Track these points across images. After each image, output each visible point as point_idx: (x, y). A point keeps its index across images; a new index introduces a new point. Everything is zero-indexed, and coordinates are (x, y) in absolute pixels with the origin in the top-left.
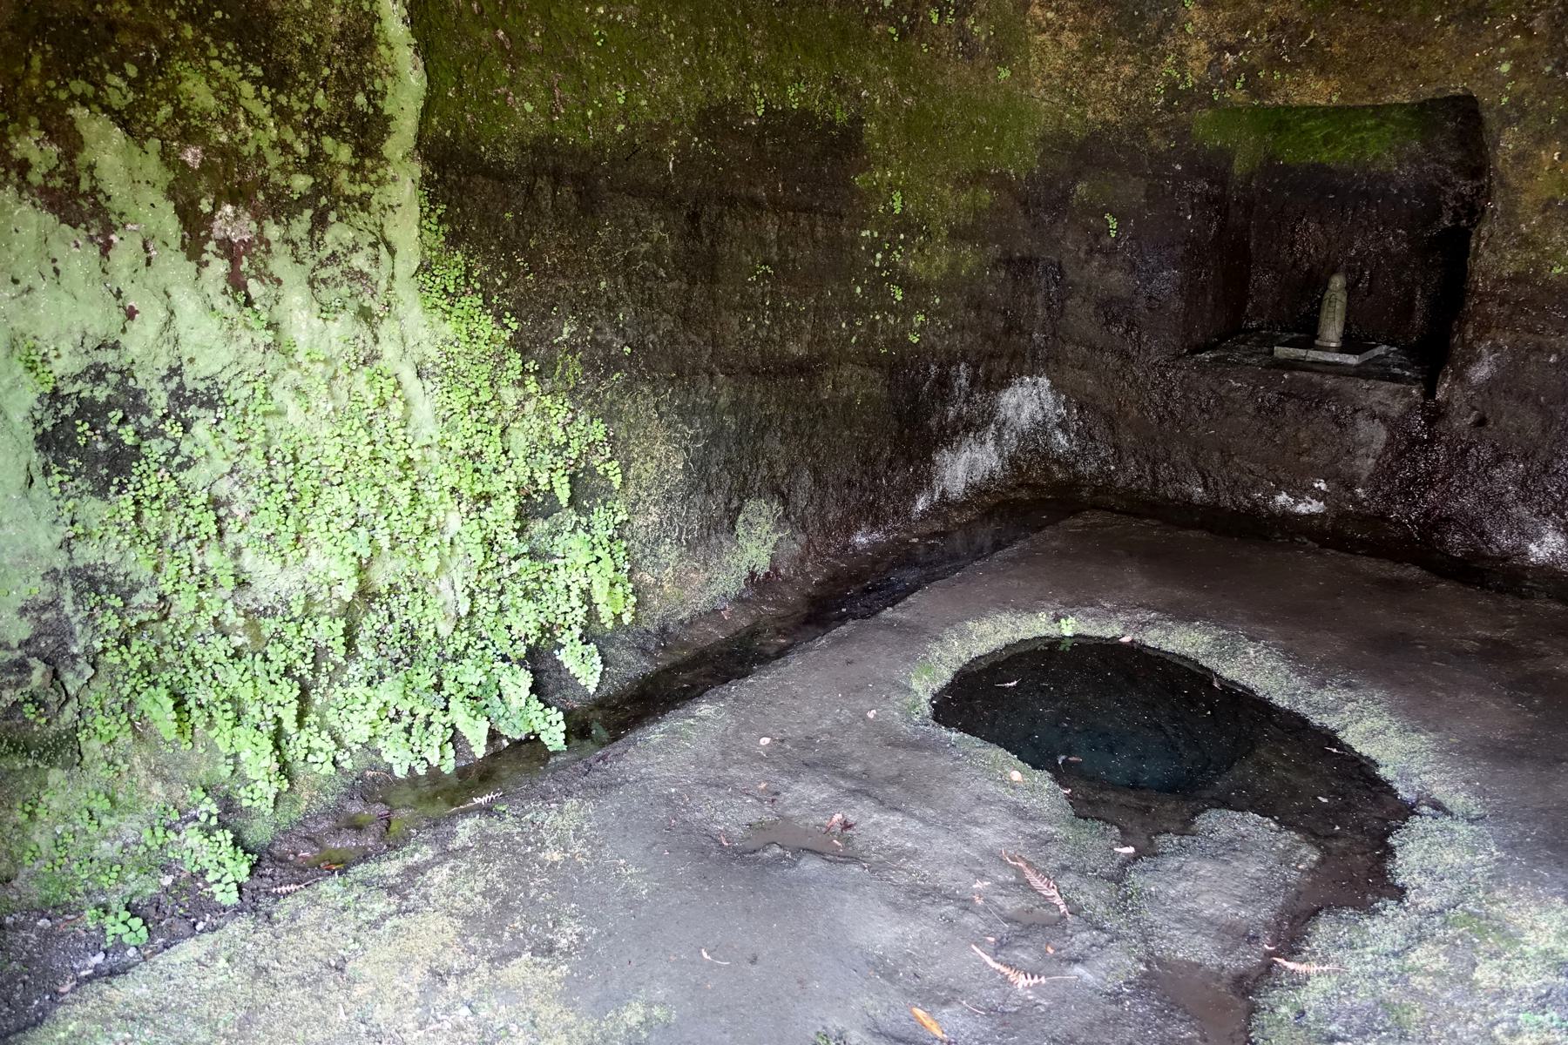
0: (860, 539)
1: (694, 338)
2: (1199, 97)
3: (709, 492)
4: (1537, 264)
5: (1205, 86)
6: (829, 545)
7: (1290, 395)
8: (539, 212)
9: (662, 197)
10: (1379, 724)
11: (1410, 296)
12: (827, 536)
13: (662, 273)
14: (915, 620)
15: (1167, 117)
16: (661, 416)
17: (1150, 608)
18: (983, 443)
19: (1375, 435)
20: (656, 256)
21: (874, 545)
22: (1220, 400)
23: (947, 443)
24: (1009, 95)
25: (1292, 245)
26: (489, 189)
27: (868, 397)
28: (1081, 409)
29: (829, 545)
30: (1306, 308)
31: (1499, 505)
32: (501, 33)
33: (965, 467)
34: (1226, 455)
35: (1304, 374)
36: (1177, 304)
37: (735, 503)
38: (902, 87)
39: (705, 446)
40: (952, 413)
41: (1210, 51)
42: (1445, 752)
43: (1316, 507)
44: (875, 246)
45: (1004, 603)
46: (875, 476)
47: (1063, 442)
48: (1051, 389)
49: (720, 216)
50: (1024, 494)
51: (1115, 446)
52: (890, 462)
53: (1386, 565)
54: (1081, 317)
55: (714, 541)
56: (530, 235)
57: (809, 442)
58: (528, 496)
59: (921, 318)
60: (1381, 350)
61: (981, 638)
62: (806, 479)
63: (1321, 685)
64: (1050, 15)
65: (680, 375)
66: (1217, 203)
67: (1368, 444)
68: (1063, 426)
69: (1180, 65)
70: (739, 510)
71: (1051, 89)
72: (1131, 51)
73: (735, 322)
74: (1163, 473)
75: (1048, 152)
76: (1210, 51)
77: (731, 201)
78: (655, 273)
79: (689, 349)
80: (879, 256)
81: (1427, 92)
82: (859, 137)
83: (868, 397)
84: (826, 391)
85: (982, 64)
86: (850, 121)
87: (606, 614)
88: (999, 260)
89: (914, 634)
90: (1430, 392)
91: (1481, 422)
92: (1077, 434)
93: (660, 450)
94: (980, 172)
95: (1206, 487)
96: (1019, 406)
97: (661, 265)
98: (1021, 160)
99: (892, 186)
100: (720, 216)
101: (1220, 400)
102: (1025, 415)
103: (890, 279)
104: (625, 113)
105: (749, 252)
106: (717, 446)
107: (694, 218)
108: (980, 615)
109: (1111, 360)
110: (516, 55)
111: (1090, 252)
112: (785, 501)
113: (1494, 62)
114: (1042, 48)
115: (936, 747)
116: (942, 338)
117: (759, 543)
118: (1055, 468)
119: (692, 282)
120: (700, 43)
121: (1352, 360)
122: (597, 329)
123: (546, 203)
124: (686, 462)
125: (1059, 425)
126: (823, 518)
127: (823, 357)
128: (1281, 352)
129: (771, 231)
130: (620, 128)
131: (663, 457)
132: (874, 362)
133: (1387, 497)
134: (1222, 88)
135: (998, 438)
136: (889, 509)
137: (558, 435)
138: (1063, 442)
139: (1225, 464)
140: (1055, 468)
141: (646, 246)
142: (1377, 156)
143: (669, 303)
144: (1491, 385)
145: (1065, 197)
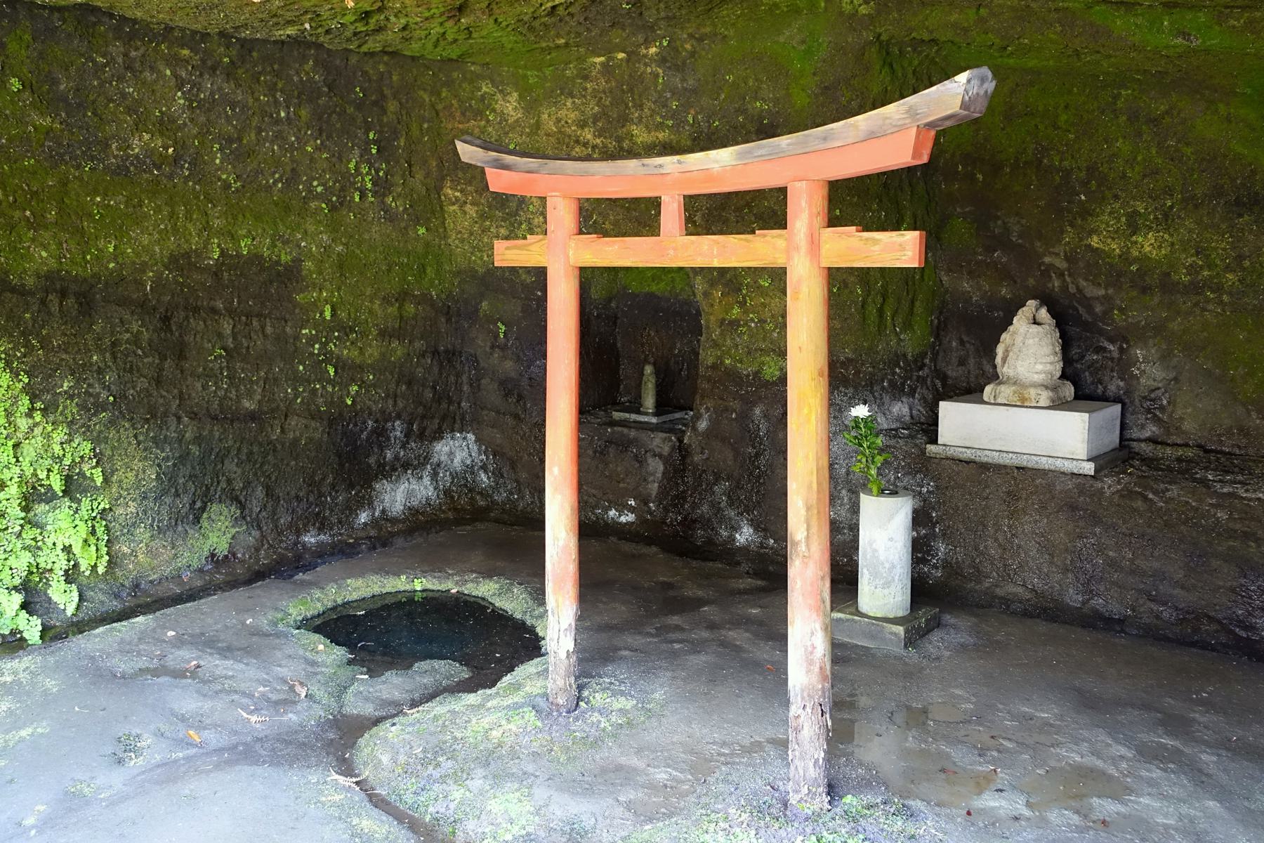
1: (165, 394)
3: (177, 495)
6: (281, 541)
7: (611, 442)
8: (49, 313)
9: (142, 307)
13: (140, 352)
16: (139, 443)
17: (472, 571)
18: (421, 478)
19: (656, 467)
20: (136, 340)
23: (387, 476)
26: (14, 300)
27: (311, 439)
28: (494, 456)
32: (28, 213)
33: (400, 495)
35: (620, 429)
37: (199, 504)
39: (174, 465)
40: (389, 455)
43: (627, 518)
44: (311, 341)
46: (321, 495)
49: (187, 318)
51: (517, 481)
52: (333, 486)
55: (180, 528)
56: (43, 327)
57: (261, 467)
58: (34, 488)
62: (260, 492)
64: (458, 194)
65: (154, 416)
68: (484, 467)
70: (203, 509)
72: (504, 220)
73: (199, 386)
77: (196, 310)
78: (134, 352)
79: (161, 401)
80: (317, 346)
82: (299, 271)
83: (311, 439)
85: (403, 225)
86: (293, 261)
87: (84, 566)
88: (426, 351)
93: (138, 465)
97: (138, 347)
100: (187, 318)
102: (457, 460)
104: (115, 257)
105: (210, 341)
106: (184, 465)
107: (166, 319)
109: (509, 420)
110: (37, 224)
111: (492, 347)
112: (242, 507)
117: (220, 533)
119: (163, 358)
120: (172, 215)
122: (89, 385)
123: (55, 308)
124: (158, 475)
125: (482, 467)
128: (617, 415)
129: (227, 327)
130: (112, 265)
131: (138, 471)
135: (434, 476)
136: (334, 520)
137: (57, 449)
141: (128, 335)
142: (682, 289)
143: (145, 371)
144: (708, 434)
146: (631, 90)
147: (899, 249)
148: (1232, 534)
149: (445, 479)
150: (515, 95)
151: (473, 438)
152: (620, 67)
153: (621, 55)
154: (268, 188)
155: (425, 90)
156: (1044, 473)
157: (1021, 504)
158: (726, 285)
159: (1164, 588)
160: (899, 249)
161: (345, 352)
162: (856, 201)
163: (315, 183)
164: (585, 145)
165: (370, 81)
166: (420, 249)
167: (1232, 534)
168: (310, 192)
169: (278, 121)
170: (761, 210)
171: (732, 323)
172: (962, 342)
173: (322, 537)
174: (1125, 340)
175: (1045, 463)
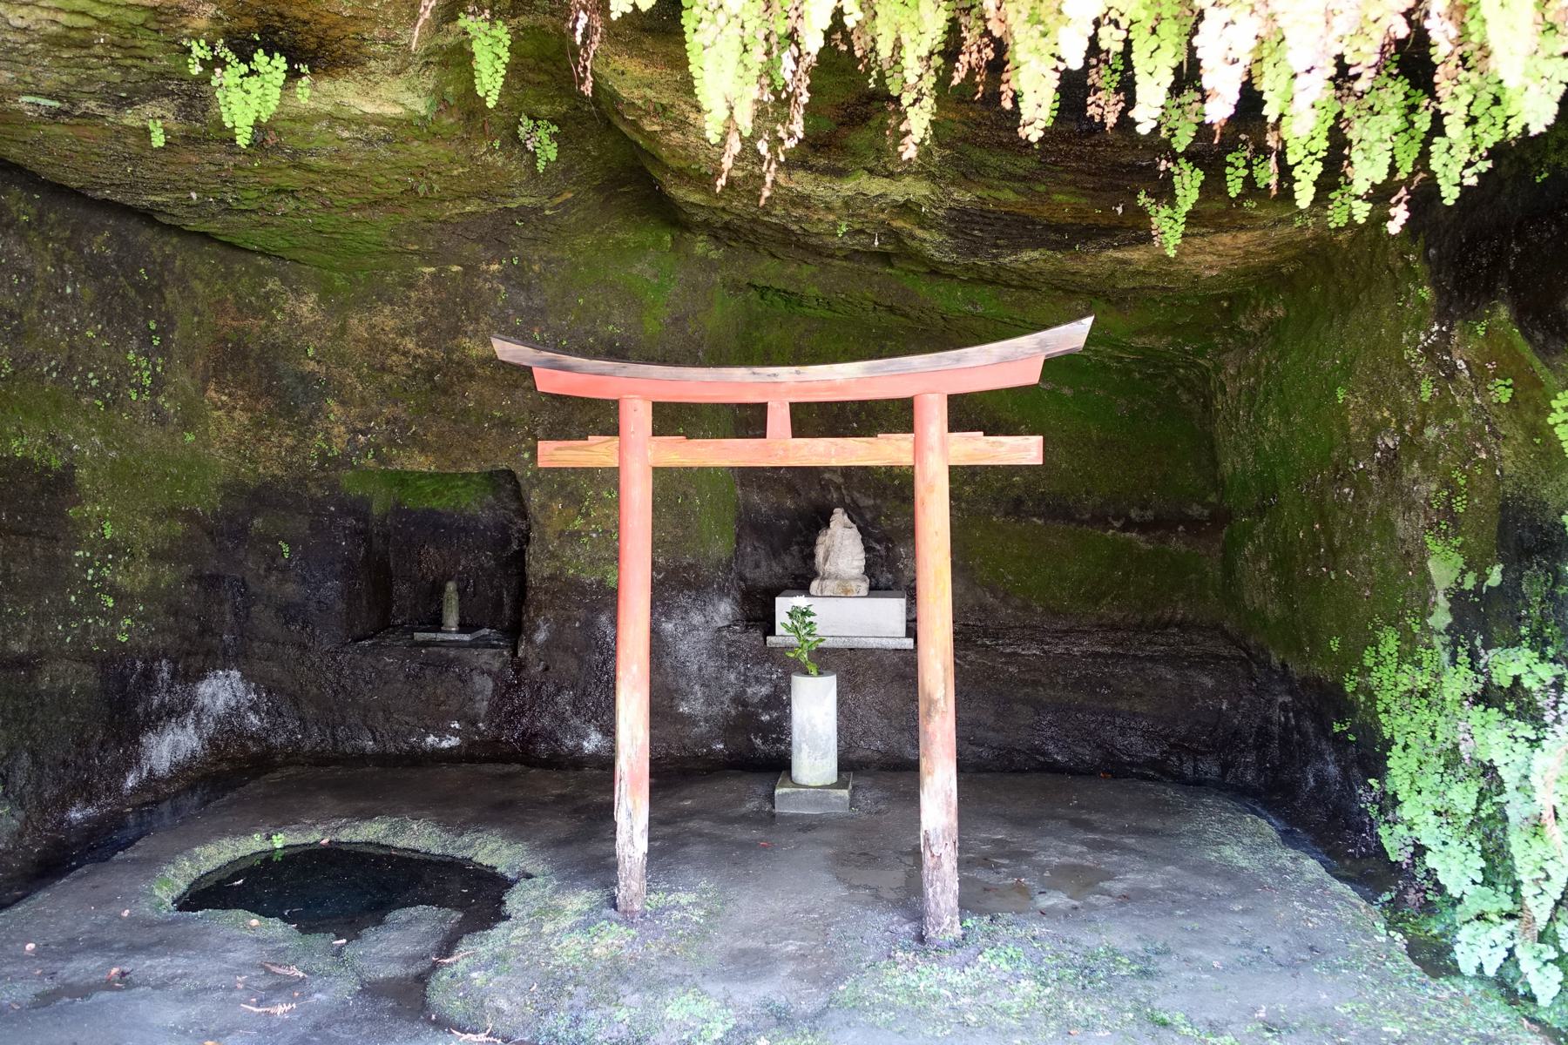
0: (75, 815)
2: (342, 462)
4: (560, 568)
5: (345, 454)
6: (46, 821)
7: (428, 664)
10: (495, 846)
11: (500, 595)
12: (43, 812)
14: (147, 855)
15: (321, 474)
17: (340, 817)
18: (184, 727)
19: (485, 685)
21: (88, 819)
22: (379, 673)
24: (194, 453)
25: (420, 563)
27: (81, 688)
28: (269, 693)
29: (46, 821)
30: (434, 608)
31: (563, 720)
33: (169, 748)
34: (387, 711)
36: (340, 606)
38: (107, 443)
40: (156, 701)
41: (348, 432)
42: (532, 851)
44: (87, 563)
45: (222, 832)
46: (89, 757)
47: (256, 721)
48: (241, 679)
50: (225, 766)
52: (102, 745)
53: (500, 766)
54: (265, 619)
59: (128, 621)
60: (486, 631)
61: (207, 859)
62: (25, 760)
63: (461, 834)
66: (361, 535)
67: (481, 692)
68: (254, 708)
69: (327, 440)
71: (227, 450)
72: (290, 428)
74: (340, 734)
75: (227, 495)
76: (348, 432)
80: (91, 571)
81: (487, 467)
84: (44, 682)
85: (171, 429)
86: (64, 467)
89: (150, 865)
90: (515, 654)
91: (546, 669)
92: (268, 713)
94: (173, 509)
95: (375, 740)
96: (214, 695)
98: (207, 501)
99: (101, 518)
101: (379, 673)
103: (100, 590)
108: (204, 841)
109: (292, 651)
111: (269, 569)
113: (520, 452)
114: (219, 421)
115: (187, 921)
116: (146, 639)
118: (250, 743)
121: (466, 638)
125: (250, 708)
126: (39, 796)
127: (41, 654)
128: (419, 636)
132: (88, 658)
133: (498, 726)
134: (359, 457)
135: (198, 722)
138: (256, 721)
139: (387, 720)
140: (250, 743)
144: (548, 644)
145: (244, 529)
146: (465, 303)
147: (1025, 450)
148: (1025, 683)
149: (210, 726)
150: (314, 296)
151: (238, 675)
152: (453, 279)
153: (456, 268)
154: (40, 377)
155: (201, 279)
156: (871, 651)
157: (859, 680)
158: (565, 497)
159: (980, 733)
160: (1025, 450)
161: (119, 578)
162: (969, 413)
163: (91, 375)
164: (405, 354)
165: (154, 262)
166: (187, 458)
167: (1025, 683)
168: (84, 385)
169: (62, 298)
170: (895, 415)
171: (571, 534)
172: (755, 548)
173: (90, 810)
174: (890, 540)
175: (873, 643)
